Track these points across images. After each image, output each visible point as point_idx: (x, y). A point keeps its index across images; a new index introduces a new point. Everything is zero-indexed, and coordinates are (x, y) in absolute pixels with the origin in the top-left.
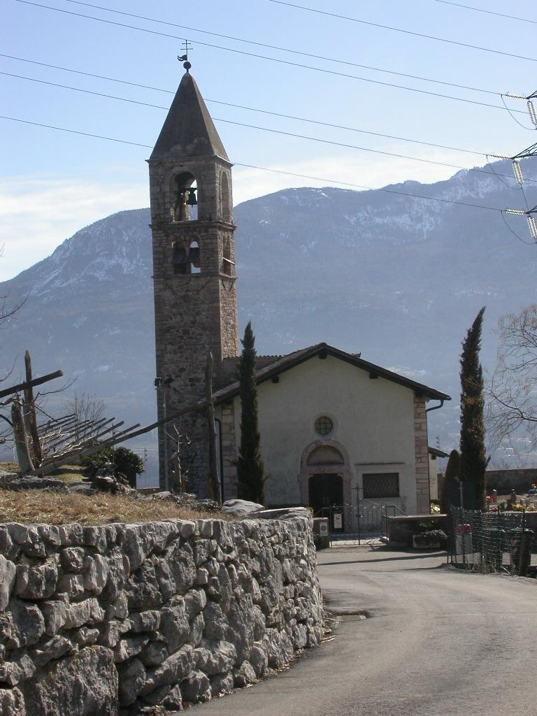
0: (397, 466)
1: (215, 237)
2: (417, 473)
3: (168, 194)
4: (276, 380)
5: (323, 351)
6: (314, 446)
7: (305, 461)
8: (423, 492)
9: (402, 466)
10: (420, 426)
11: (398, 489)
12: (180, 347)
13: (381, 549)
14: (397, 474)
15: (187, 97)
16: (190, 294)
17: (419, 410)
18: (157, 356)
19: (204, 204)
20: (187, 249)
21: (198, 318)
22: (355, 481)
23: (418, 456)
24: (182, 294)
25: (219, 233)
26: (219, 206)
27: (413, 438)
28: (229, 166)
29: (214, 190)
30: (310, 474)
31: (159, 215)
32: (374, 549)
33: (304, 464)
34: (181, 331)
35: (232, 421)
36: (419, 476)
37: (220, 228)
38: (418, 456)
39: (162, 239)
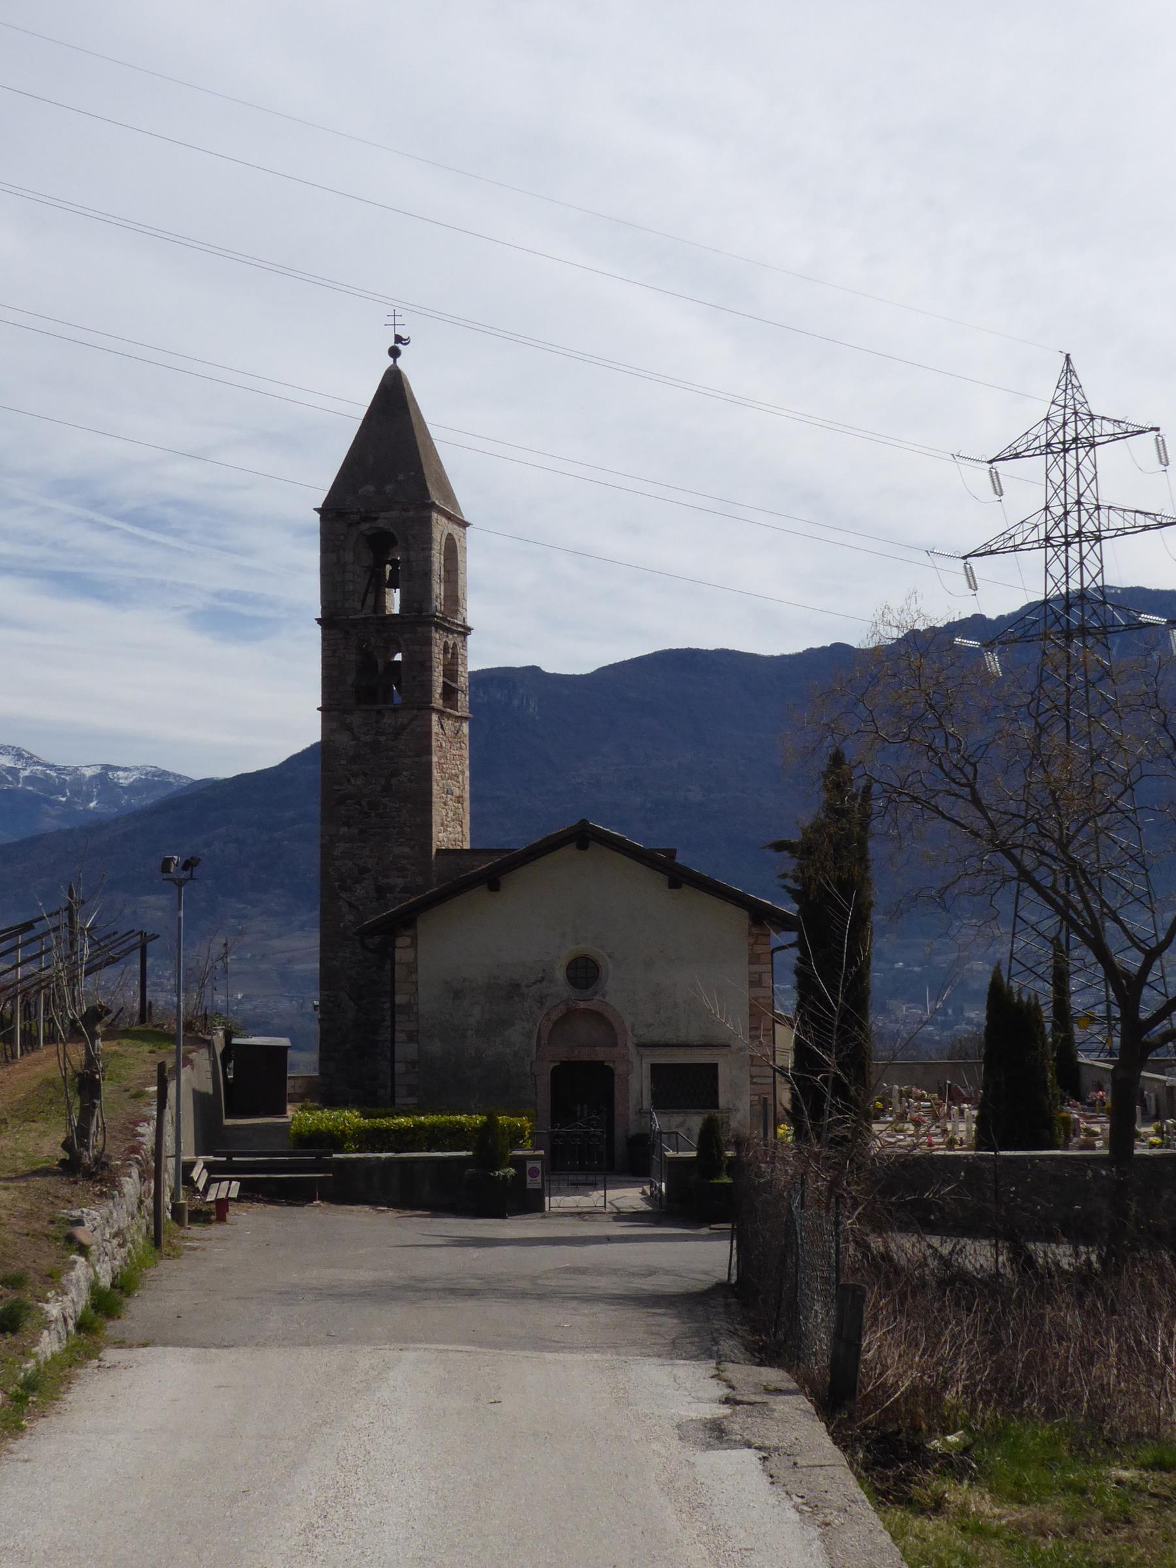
1: (429, 642)
2: (752, 1065)
4: (494, 886)
5: (582, 837)
9: (725, 1051)
15: (393, 404)
16: (382, 739)
17: (759, 949)
18: (323, 846)
20: (380, 661)
21: (394, 781)
22: (637, 1086)
24: (369, 738)
25: (436, 635)
26: (438, 589)
28: (464, 525)
29: (428, 561)
32: (620, 1216)
34: (364, 803)
37: (439, 627)
38: (753, 1033)
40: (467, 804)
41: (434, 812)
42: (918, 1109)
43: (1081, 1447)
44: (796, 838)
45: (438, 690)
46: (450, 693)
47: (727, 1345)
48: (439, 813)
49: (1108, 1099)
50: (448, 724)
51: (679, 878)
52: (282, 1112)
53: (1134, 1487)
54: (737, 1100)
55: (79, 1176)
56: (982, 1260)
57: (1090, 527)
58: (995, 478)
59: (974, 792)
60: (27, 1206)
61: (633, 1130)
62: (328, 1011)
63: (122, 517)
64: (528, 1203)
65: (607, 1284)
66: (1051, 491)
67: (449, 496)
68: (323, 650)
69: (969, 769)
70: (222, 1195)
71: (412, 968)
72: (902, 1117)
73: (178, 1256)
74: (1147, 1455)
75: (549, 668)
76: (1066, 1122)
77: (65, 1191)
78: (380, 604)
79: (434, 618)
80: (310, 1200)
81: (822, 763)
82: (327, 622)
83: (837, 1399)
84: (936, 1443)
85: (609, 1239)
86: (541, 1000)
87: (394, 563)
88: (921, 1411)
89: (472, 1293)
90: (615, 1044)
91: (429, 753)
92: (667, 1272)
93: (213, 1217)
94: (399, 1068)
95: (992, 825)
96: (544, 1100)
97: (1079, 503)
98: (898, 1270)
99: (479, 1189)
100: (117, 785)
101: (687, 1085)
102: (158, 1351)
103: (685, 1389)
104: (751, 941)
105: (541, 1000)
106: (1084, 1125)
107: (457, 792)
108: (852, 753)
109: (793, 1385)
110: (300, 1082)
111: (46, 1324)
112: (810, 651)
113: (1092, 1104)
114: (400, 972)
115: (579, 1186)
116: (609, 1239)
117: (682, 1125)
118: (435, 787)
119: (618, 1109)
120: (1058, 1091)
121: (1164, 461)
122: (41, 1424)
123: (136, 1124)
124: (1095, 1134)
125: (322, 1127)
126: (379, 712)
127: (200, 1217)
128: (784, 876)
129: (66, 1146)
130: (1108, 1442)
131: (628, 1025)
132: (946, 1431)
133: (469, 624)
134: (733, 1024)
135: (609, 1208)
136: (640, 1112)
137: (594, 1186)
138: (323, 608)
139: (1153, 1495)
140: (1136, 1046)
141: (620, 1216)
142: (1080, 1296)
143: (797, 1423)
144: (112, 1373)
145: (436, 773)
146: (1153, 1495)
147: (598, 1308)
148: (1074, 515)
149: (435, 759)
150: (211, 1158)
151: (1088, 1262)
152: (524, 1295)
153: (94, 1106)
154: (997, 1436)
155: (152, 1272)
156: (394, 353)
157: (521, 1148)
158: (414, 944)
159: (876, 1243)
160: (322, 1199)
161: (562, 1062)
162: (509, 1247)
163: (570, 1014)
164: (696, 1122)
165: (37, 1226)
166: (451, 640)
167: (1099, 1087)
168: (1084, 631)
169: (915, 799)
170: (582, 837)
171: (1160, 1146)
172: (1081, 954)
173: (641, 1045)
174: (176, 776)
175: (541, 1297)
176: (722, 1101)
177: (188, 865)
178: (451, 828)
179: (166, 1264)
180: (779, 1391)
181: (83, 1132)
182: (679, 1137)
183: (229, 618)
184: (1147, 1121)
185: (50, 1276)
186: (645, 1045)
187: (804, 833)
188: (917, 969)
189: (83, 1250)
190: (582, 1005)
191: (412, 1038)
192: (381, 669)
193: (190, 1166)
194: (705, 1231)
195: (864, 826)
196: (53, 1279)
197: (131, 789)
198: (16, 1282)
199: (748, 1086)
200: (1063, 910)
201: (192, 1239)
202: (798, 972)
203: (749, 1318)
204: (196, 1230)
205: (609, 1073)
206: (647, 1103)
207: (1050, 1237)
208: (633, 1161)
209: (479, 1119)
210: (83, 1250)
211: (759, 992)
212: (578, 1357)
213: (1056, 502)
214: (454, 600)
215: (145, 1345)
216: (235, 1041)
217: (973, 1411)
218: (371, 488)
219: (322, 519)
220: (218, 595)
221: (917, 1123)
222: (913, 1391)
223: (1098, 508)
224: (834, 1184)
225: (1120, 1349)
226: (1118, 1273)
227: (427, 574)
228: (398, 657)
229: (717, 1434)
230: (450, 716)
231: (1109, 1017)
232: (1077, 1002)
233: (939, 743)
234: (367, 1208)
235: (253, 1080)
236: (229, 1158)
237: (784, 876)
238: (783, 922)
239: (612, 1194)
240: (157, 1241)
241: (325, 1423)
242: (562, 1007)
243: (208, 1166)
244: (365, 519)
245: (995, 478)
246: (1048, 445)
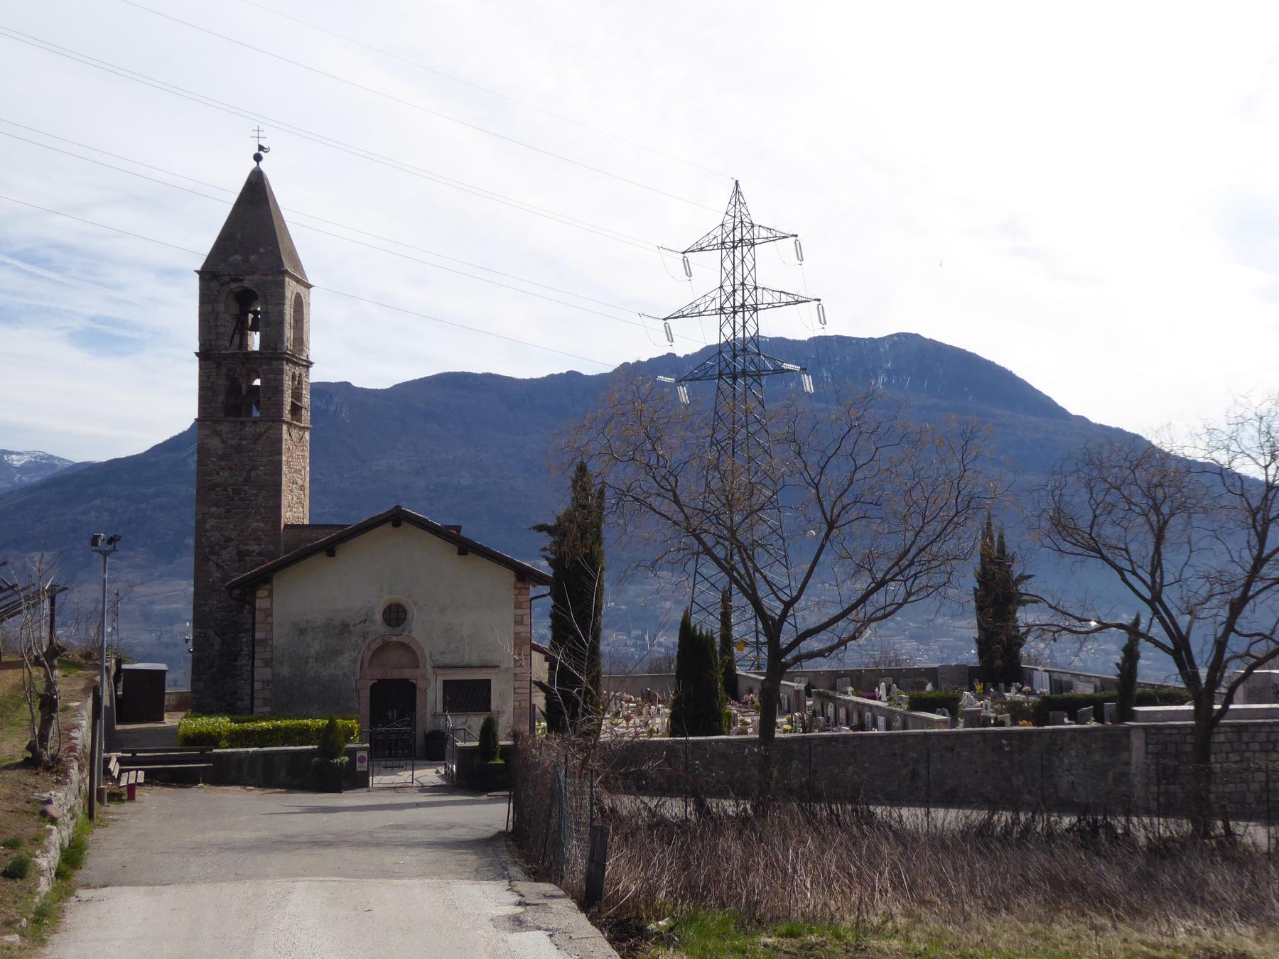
0: (490, 671)
1: (281, 372)
5: (397, 518)
6: (380, 641)
7: (366, 661)
9: (496, 670)
12: (228, 511)
13: (435, 789)
15: (256, 195)
16: (244, 443)
17: (522, 598)
20: (244, 387)
22: (432, 695)
24: (234, 442)
26: (289, 333)
28: (309, 286)
29: (282, 313)
32: (423, 789)
33: (366, 665)
37: (289, 361)
40: (307, 492)
41: (283, 498)
42: (628, 708)
43: (743, 926)
44: (552, 522)
45: (287, 408)
46: (296, 410)
47: (514, 871)
48: (286, 498)
49: (756, 700)
50: (295, 432)
51: (466, 548)
52: (161, 719)
53: (775, 948)
54: (504, 703)
55: (40, 769)
56: (676, 810)
57: (750, 301)
58: (686, 263)
59: (675, 496)
60: (7, 791)
61: (430, 728)
62: (200, 642)
63: (12, 256)
64: (359, 781)
65: (420, 835)
66: (724, 275)
67: (297, 264)
69: (672, 480)
70: (132, 781)
71: (268, 613)
72: (617, 714)
73: (107, 826)
74: (783, 929)
75: (357, 384)
76: (729, 715)
77: (31, 780)
78: (243, 343)
79: (283, 354)
80: (196, 783)
81: (571, 473)
82: (204, 355)
83: (590, 899)
84: (652, 926)
85: (418, 805)
86: (364, 636)
87: (256, 313)
88: (642, 906)
89: (330, 844)
90: (417, 667)
91: (280, 453)
92: (462, 826)
93: (125, 797)
94: (257, 686)
95: (687, 518)
96: (365, 709)
97: (743, 284)
98: (621, 820)
99: (323, 772)
100: (11, 466)
101: (469, 695)
102: (116, 889)
103: (490, 898)
105: (364, 636)
106: (740, 718)
107: (300, 482)
108: (593, 467)
109: (562, 892)
110: (173, 697)
111: (41, 873)
112: (552, 376)
113: (746, 703)
114: (259, 616)
115: (393, 769)
116: (418, 805)
118: (284, 478)
120: (724, 695)
121: (800, 258)
122: (56, 938)
123: (70, 730)
124: (747, 724)
125: (203, 729)
126: (242, 423)
127: (115, 797)
128: (544, 549)
129: (30, 747)
130: (759, 922)
131: (427, 653)
132: (658, 919)
133: (311, 359)
134: (506, 651)
135: (415, 784)
136: (435, 715)
137: (401, 768)
138: (201, 345)
139: (786, 952)
140: (777, 667)
141: (423, 789)
142: (740, 832)
143: (566, 913)
144: (91, 905)
145: (285, 469)
146: (786, 952)
147: (419, 851)
148: (740, 292)
149: (284, 458)
150: (120, 754)
151: (745, 810)
152: (365, 844)
153: (52, 718)
154: (692, 920)
155: (91, 838)
156: (258, 158)
157: (352, 742)
158: (270, 596)
159: (607, 802)
160: (205, 782)
162: (342, 811)
163: (385, 646)
164: (476, 722)
165: (18, 805)
166: (297, 371)
167: (750, 691)
168: (744, 373)
169: (637, 500)
170: (397, 518)
171: (791, 731)
172: (739, 599)
174: (60, 459)
175: (378, 845)
176: (493, 706)
177: (111, 541)
178: (295, 508)
179: (98, 831)
180: (553, 897)
181: (43, 737)
182: (466, 732)
183: (102, 337)
184: (783, 714)
185: (35, 839)
187: (558, 518)
188: (623, 607)
189: (54, 821)
190: (394, 639)
191: (268, 663)
192: (244, 392)
193: (107, 761)
194: (484, 797)
195: (600, 518)
196: (37, 841)
197: (24, 469)
198: (13, 844)
199: (512, 695)
200: (729, 570)
201: (112, 814)
202: (553, 616)
203: (527, 851)
204: (113, 807)
205: (414, 687)
206: (439, 709)
207: (723, 795)
208: (433, 749)
209: (321, 723)
210: (54, 821)
211: (522, 629)
212: (415, 881)
213: (727, 283)
214: (300, 341)
215: (105, 886)
216: (124, 666)
217: (675, 905)
218: (238, 257)
219: (201, 279)
220: (93, 319)
221: (628, 719)
222: (637, 894)
223: (756, 288)
224: (584, 762)
225: (766, 865)
226: (764, 816)
227: (280, 323)
228: (257, 382)
229: (518, 923)
230: (296, 426)
231: (757, 642)
232: (737, 632)
233: (653, 461)
234: (238, 788)
235: (140, 696)
236: (134, 754)
237: (544, 549)
238: (540, 579)
239: (417, 773)
240: (91, 816)
241: (257, 928)
243: (119, 760)
244: (233, 281)
245: (686, 263)
246: (723, 243)
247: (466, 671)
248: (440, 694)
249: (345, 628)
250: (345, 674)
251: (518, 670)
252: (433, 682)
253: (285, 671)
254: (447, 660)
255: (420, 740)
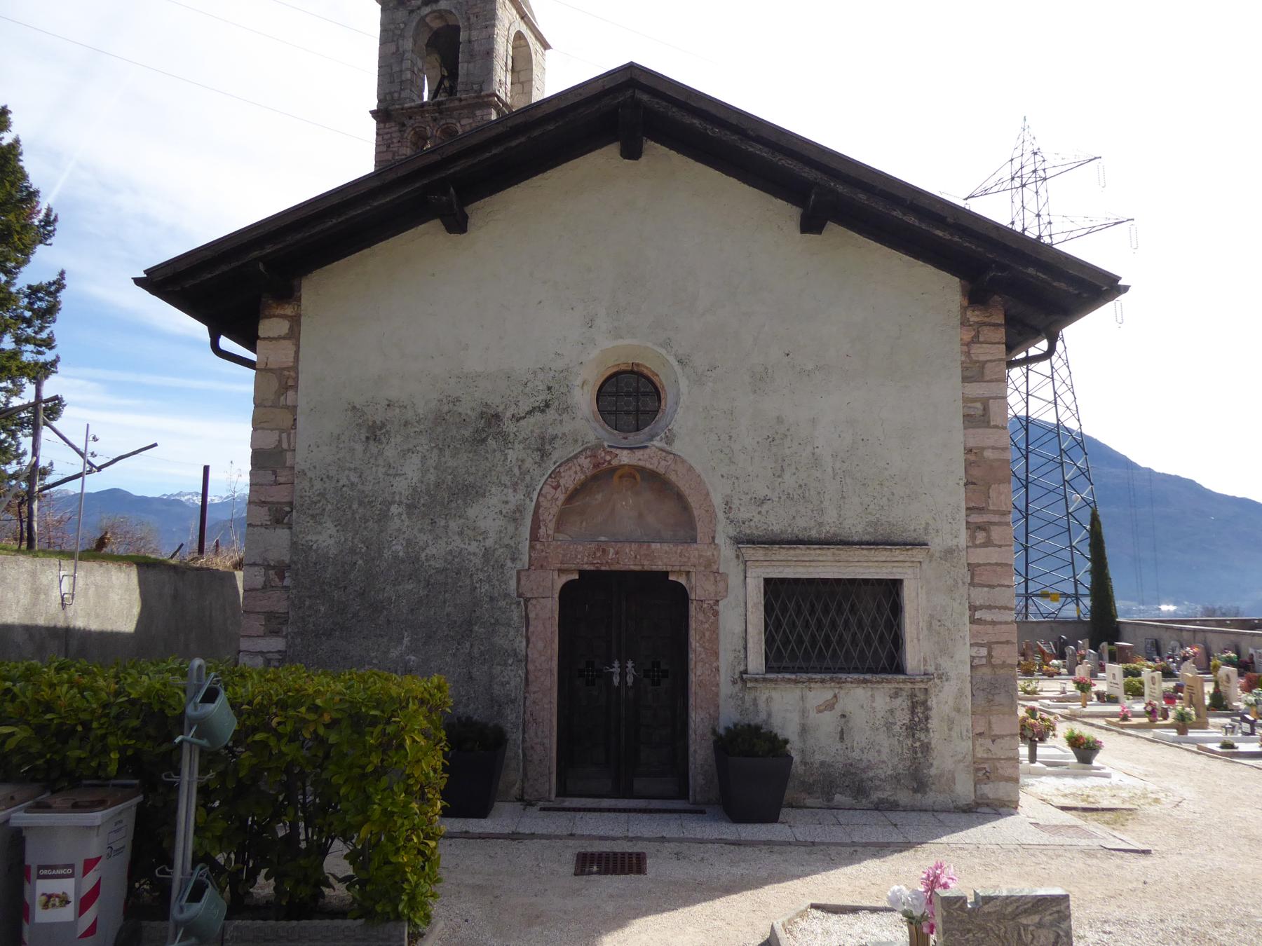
0: (898, 554)
2: (972, 584)
3: (408, 55)
7: (550, 515)
8: (995, 661)
9: (918, 554)
10: (986, 409)
11: (897, 642)
14: (894, 587)
19: (471, 65)
22: (732, 625)
23: (976, 518)
27: (960, 457)
30: (561, 571)
31: (391, 93)
35: (289, 361)
36: (980, 596)
38: (976, 518)
39: (391, 138)
61: (729, 715)
68: (377, 146)
104: (967, 338)
117: (830, 706)
119: (697, 672)
131: (717, 500)
136: (743, 678)
158: (294, 335)
161: (581, 573)
163: (603, 476)
173: (743, 541)
176: (915, 653)
186: (752, 541)
190: (625, 458)
199: (967, 628)
205: (677, 598)
206: (756, 662)
242: (585, 462)
247: (828, 553)
248: (757, 618)
249: (489, 425)
250: (487, 554)
251: (980, 556)
252: (734, 580)
253: (325, 537)
254: (776, 521)
255: (700, 752)
